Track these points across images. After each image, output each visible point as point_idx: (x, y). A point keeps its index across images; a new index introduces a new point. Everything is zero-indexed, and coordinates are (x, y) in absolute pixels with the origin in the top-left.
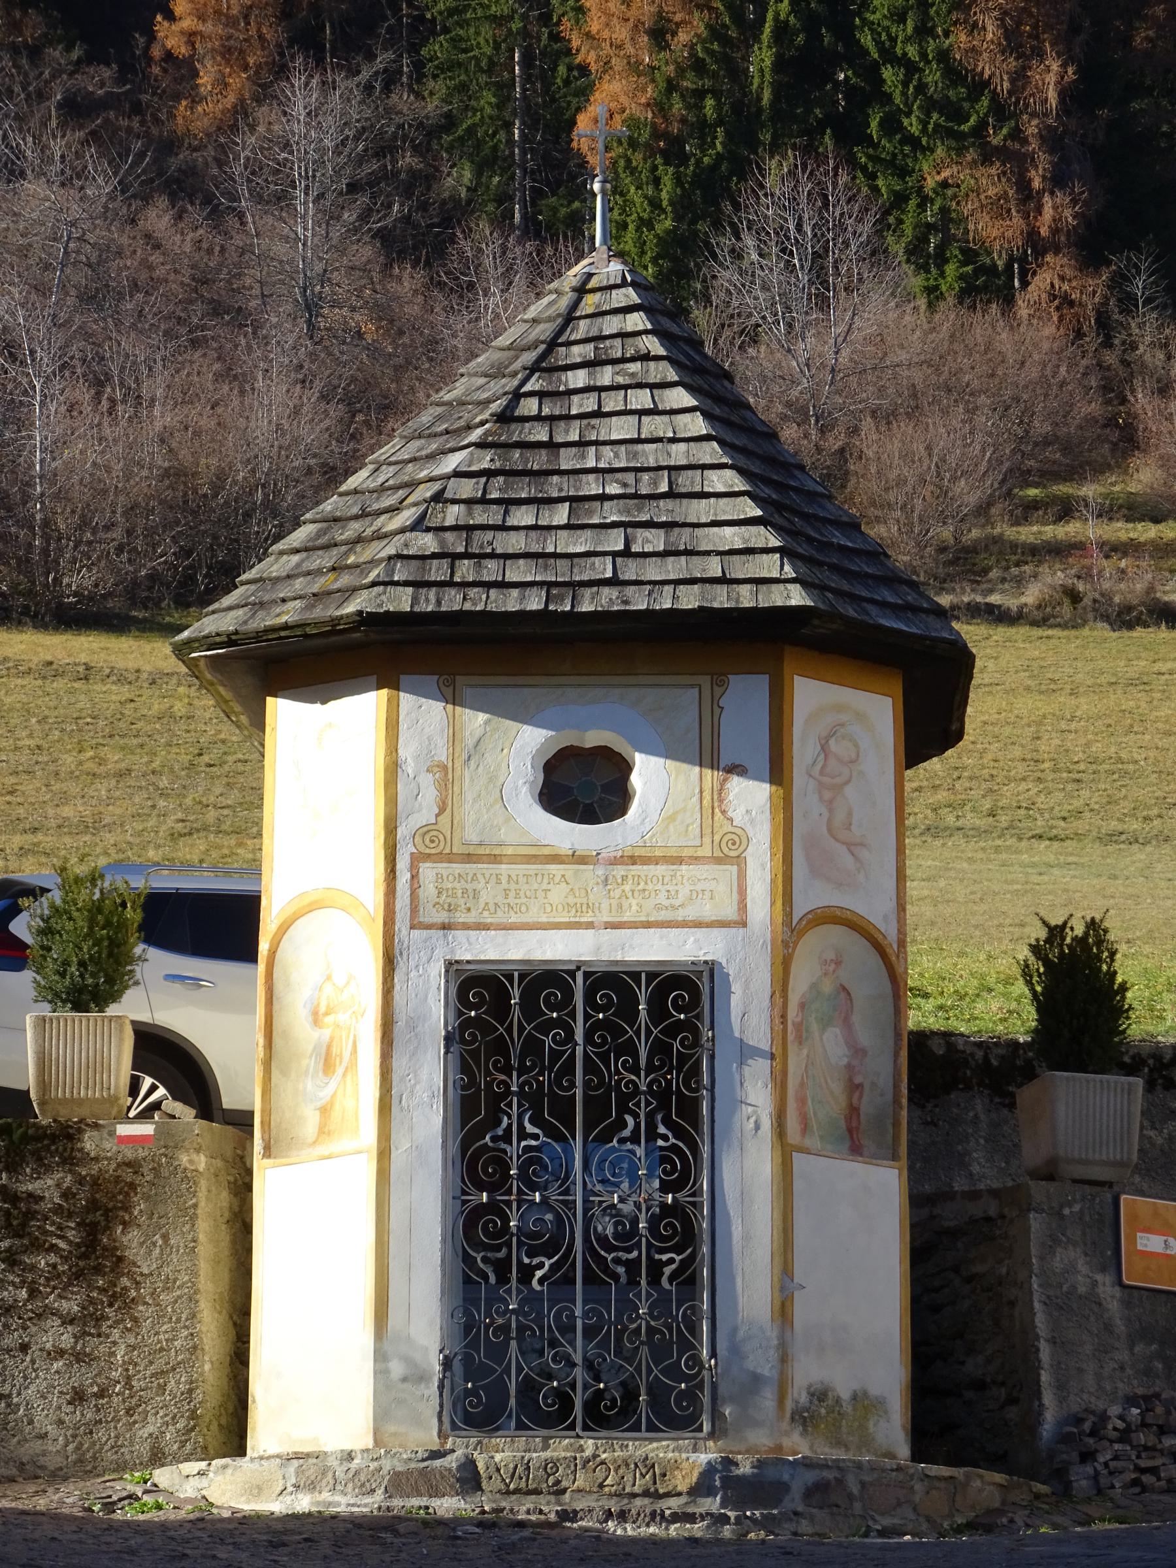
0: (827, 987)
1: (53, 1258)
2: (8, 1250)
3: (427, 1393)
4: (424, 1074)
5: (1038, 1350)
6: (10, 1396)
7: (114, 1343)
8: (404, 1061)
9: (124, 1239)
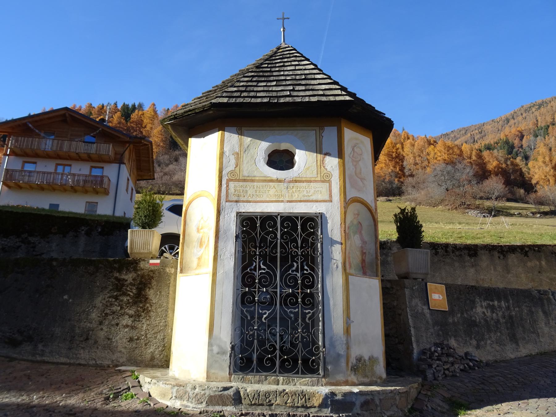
0: (355, 222)
1: (128, 298)
2: (116, 295)
3: (225, 358)
4: (228, 248)
5: (410, 330)
6: (112, 339)
7: (143, 324)
8: (222, 244)
9: (149, 293)
